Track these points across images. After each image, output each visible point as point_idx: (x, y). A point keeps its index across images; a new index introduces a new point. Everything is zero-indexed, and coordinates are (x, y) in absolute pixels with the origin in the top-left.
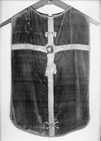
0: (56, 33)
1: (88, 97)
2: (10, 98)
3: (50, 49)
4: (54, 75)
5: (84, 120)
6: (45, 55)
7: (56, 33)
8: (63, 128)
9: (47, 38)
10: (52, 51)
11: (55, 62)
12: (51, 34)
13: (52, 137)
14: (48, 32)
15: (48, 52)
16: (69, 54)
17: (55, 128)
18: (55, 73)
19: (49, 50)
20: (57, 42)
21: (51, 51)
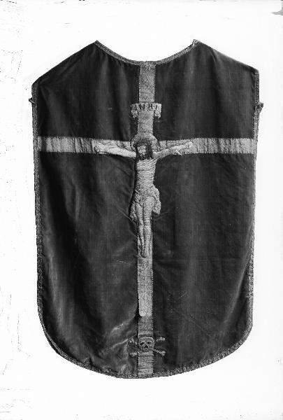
0: (160, 105)
1: (246, 275)
2: (256, 194)
3: (143, 150)
4: (153, 214)
5: (235, 330)
6: (161, 163)
7: (160, 105)
8: (174, 359)
9: (137, 118)
10: (149, 155)
11: (157, 183)
12: (149, 110)
13: (147, 376)
14: (138, 102)
15: (139, 158)
16: (175, 163)
17: (155, 353)
18: (158, 211)
19: (140, 152)
20: (166, 129)
21: (145, 155)
